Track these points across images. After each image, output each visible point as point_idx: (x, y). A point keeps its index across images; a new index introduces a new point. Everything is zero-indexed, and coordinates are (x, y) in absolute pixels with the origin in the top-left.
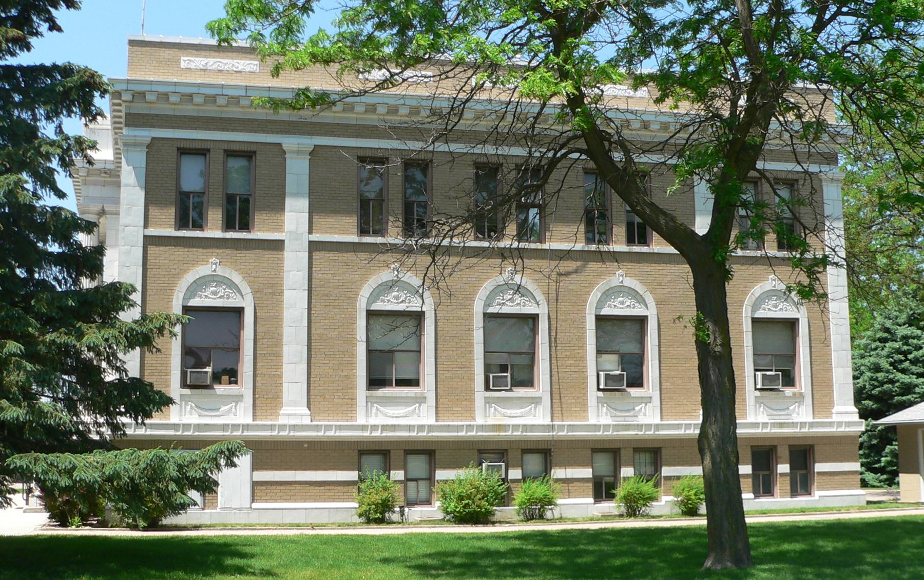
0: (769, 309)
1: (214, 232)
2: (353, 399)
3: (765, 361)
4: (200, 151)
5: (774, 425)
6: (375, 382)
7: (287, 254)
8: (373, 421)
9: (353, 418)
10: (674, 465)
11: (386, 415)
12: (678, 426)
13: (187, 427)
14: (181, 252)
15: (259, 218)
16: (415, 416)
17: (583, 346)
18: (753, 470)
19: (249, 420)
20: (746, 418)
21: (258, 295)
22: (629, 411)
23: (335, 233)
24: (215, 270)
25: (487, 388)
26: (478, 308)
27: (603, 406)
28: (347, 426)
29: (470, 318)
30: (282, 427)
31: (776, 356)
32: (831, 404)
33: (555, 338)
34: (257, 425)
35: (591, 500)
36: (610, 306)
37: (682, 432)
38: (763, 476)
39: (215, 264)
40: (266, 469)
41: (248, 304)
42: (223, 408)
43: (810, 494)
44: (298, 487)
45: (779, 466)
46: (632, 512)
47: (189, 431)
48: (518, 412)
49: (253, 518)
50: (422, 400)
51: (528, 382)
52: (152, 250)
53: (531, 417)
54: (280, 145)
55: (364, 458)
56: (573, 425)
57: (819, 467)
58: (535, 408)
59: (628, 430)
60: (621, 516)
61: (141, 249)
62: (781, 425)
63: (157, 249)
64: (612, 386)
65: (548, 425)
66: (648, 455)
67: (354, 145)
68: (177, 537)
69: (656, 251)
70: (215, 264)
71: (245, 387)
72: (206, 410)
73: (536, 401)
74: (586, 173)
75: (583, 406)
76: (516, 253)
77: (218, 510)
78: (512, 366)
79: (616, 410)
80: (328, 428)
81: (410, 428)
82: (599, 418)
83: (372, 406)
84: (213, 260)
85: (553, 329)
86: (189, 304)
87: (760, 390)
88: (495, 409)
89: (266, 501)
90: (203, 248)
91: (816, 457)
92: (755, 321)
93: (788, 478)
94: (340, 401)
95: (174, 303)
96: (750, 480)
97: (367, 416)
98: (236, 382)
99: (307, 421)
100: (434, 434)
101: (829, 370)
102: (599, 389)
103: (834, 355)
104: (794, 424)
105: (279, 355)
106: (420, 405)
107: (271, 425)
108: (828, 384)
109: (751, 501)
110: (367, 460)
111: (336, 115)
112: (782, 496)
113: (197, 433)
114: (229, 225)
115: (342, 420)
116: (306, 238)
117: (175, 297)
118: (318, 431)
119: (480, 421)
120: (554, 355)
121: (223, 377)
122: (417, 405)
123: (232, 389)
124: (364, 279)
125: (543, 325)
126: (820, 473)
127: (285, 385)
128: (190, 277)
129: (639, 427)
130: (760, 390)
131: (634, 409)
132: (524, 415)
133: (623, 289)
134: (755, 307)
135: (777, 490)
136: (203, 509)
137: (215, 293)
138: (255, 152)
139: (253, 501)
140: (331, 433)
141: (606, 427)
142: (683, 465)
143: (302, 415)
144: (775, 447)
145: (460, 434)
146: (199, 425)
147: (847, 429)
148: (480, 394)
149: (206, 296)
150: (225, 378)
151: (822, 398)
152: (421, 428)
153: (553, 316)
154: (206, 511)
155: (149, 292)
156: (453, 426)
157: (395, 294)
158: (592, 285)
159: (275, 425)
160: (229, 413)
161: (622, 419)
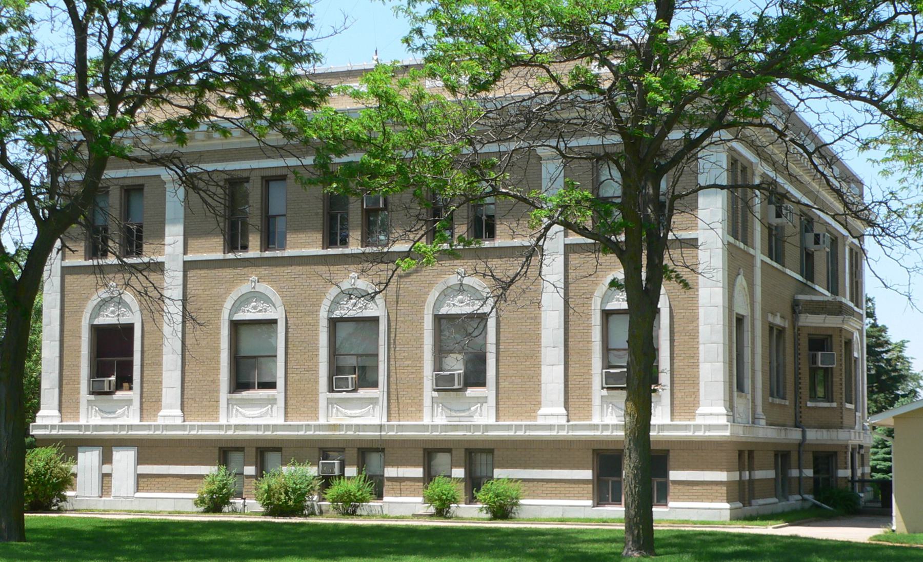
1: (254, 252)
6: (239, 383)
8: (234, 421)
9: (589, 417)
10: (507, 468)
11: (244, 416)
18: (815, 473)
20: (78, 420)
22: (464, 411)
23: (205, 252)
25: (331, 390)
26: (323, 314)
27: (438, 406)
29: (316, 324)
30: (698, 427)
32: (696, 404)
33: (395, 340)
35: (590, 503)
36: (449, 305)
37: (554, 433)
38: (613, 482)
40: (148, 464)
46: (441, 513)
49: (101, 507)
50: (272, 401)
54: (159, 176)
56: (403, 425)
57: (674, 475)
59: (245, 430)
60: (431, 516)
67: (276, 165)
68: (93, 518)
72: (106, 413)
73: (373, 401)
76: (97, 271)
77: (112, 498)
79: (451, 410)
80: (518, 427)
81: (257, 427)
82: (433, 419)
83: (333, 407)
85: (393, 330)
88: (237, 410)
89: (147, 491)
94: (207, 403)
95: (83, 323)
96: (591, 486)
99: (179, 421)
101: (696, 365)
105: (160, 364)
106: (482, 405)
107: (686, 425)
108: (694, 381)
115: (209, 420)
116: (181, 258)
118: (185, 430)
119: (322, 421)
120: (392, 356)
124: (228, 292)
126: (675, 482)
127: (164, 390)
131: (470, 409)
132: (360, 415)
133: (256, 295)
137: (255, 308)
139: (138, 490)
143: (175, 416)
146: (96, 426)
147: (707, 434)
148: (324, 395)
152: (267, 427)
153: (393, 318)
155: (66, 315)
158: (431, 285)
159: (690, 425)
160: (124, 414)
161: (457, 419)
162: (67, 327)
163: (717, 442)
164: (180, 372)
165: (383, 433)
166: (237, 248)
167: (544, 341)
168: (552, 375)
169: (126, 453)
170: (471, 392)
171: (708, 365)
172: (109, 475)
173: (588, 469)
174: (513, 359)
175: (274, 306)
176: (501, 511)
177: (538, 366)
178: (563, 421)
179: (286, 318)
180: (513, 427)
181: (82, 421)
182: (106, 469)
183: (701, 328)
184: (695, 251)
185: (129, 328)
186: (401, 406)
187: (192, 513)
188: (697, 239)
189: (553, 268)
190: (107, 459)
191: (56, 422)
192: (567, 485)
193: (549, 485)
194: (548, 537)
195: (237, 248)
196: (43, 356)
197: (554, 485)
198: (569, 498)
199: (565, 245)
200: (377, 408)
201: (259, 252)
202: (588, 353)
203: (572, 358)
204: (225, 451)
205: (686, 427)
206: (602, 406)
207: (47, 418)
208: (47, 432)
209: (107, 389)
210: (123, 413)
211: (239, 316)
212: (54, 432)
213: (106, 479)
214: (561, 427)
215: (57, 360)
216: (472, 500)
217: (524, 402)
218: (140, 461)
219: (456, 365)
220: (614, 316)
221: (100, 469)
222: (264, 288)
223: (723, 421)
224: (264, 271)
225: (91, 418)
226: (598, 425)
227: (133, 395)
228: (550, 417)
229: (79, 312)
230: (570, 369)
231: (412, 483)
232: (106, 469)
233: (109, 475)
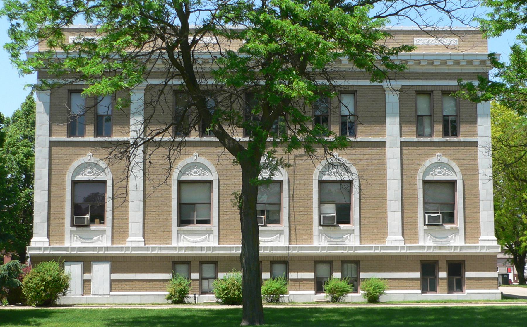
0: (435, 175)
2: (170, 232)
3: (431, 208)
4: (428, 93)
5: (435, 247)
6: (183, 221)
7: (480, 149)
8: (181, 244)
9: (170, 243)
10: (368, 272)
11: (189, 241)
12: (370, 248)
13: (73, 249)
14: (70, 150)
15: (463, 128)
16: (206, 242)
17: (311, 199)
19: (109, 245)
20: (64, 244)
21: (115, 173)
22: (339, 238)
24: (90, 160)
27: (322, 235)
28: (165, 247)
29: (64, 181)
30: (127, 249)
31: (441, 204)
32: (478, 234)
33: (293, 195)
34: (467, 246)
36: (432, 175)
38: (430, 279)
39: (90, 156)
41: (108, 177)
42: (95, 238)
43: (462, 292)
44: (137, 283)
45: (466, 273)
46: (335, 300)
47: (74, 251)
48: (269, 239)
50: (210, 232)
51: (277, 221)
52: (54, 149)
53: (277, 242)
55: (345, 265)
56: (302, 247)
57: (468, 275)
58: (455, 236)
61: (48, 149)
62: (441, 248)
63: (57, 148)
64: (326, 223)
65: (286, 247)
66: (353, 265)
69: (462, 140)
70: (90, 156)
71: (284, 226)
72: (85, 239)
73: (280, 232)
74: (443, 94)
75: (310, 237)
77: (91, 296)
78: (267, 211)
79: (331, 237)
80: (154, 249)
81: (202, 248)
82: (320, 243)
84: (438, 154)
85: (292, 189)
86: (76, 179)
87: (427, 225)
88: (184, 238)
89: (119, 291)
90: (83, 147)
91: (466, 268)
92: (425, 182)
93: (446, 281)
94: (162, 233)
96: (419, 282)
97: (178, 241)
98: (103, 223)
100: (216, 252)
101: (478, 213)
102: (425, 225)
103: (481, 203)
104: (449, 247)
107: (121, 247)
108: (477, 222)
109: (419, 295)
110: (205, 267)
111: (437, 67)
112: (442, 292)
113: (79, 253)
114: (446, 134)
116: (398, 140)
117: (67, 176)
118: (148, 250)
120: (292, 205)
121: (96, 220)
122: (349, 235)
123: (101, 227)
125: (285, 187)
126: (468, 279)
127: (130, 225)
128: (76, 164)
129: (345, 248)
130: (427, 225)
131: (343, 237)
133: (197, 164)
134: (425, 173)
135: (438, 289)
136: (83, 295)
137: (196, 172)
138: (356, 91)
139: (111, 290)
140: (155, 252)
141: (429, 247)
142: (374, 272)
144: (438, 261)
145: (203, 252)
146: (80, 248)
147: (488, 251)
149: (85, 175)
150: (97, 221)
151: (472, 230)
152: (208, 248)
153: (292, 181)
154: (84, 296)
155: (53, 173)
156: (227, 247)
157: (195, 170)
159: (123, 247)
160: (99, 239)
161: (335, 243)
162: (53, 181)
163: (491, 256)
164: (142, 213)
165: (290, 252)
166: (449, 135)
167: (389, 197)
168: (394, 217)
169: (105, 265)
170: (343, 227)
171: (485, 213)
172: (89, 280)
173: (417, 272)
174: (369, 207)
175: (210, 171)
176: (373, 299)
177: (385, 212)
178: (142, 245)
179: (219, 180)
180: (371, 248)
181: (67, 245)
182: (87, 276)
183: (480, 192)
184: (475, 148)
185: (104, 182)
186: (298, 235)
187: (165, 304)
188: (477, 142)
189: (392, 155)
190: (87, 269)
191: (47, 245)
192: (405, 282)
193: (394, 282)
194: (269, 312)
195: (449, 135)
196: (35, 201)
197: (397, 281)
198: (406, 289)
199: (401, 142)
200: (282, 236)
201: (198, 137)
202: (415, 205)
203: (405, 208)
204: (176, 264)
205: (476, 247)
206: (424, 236)
207: (39, 242)
208: (41, 252)
209: (86, 224)
210: (99, 239)
211: (184, 178)
212: (47, 252)
213: (86, 283)
214: (46, 249)
215: (47, 203)
216: (356, 291)
217: (376, 233)
218: (113, 270)
219: (331, 210)
220: (327, 184)
221: (82, 276)
222: (202, 160)
223: (495, 244)
224: (202, 149)
225: (73, 242)
226: (68, 248)
227: (107, 226)
228: (394, 242)
229: (63, 173)
230: (404, 214)
231: (308, 282)
232: (87, 276)
233: (89, 280)
